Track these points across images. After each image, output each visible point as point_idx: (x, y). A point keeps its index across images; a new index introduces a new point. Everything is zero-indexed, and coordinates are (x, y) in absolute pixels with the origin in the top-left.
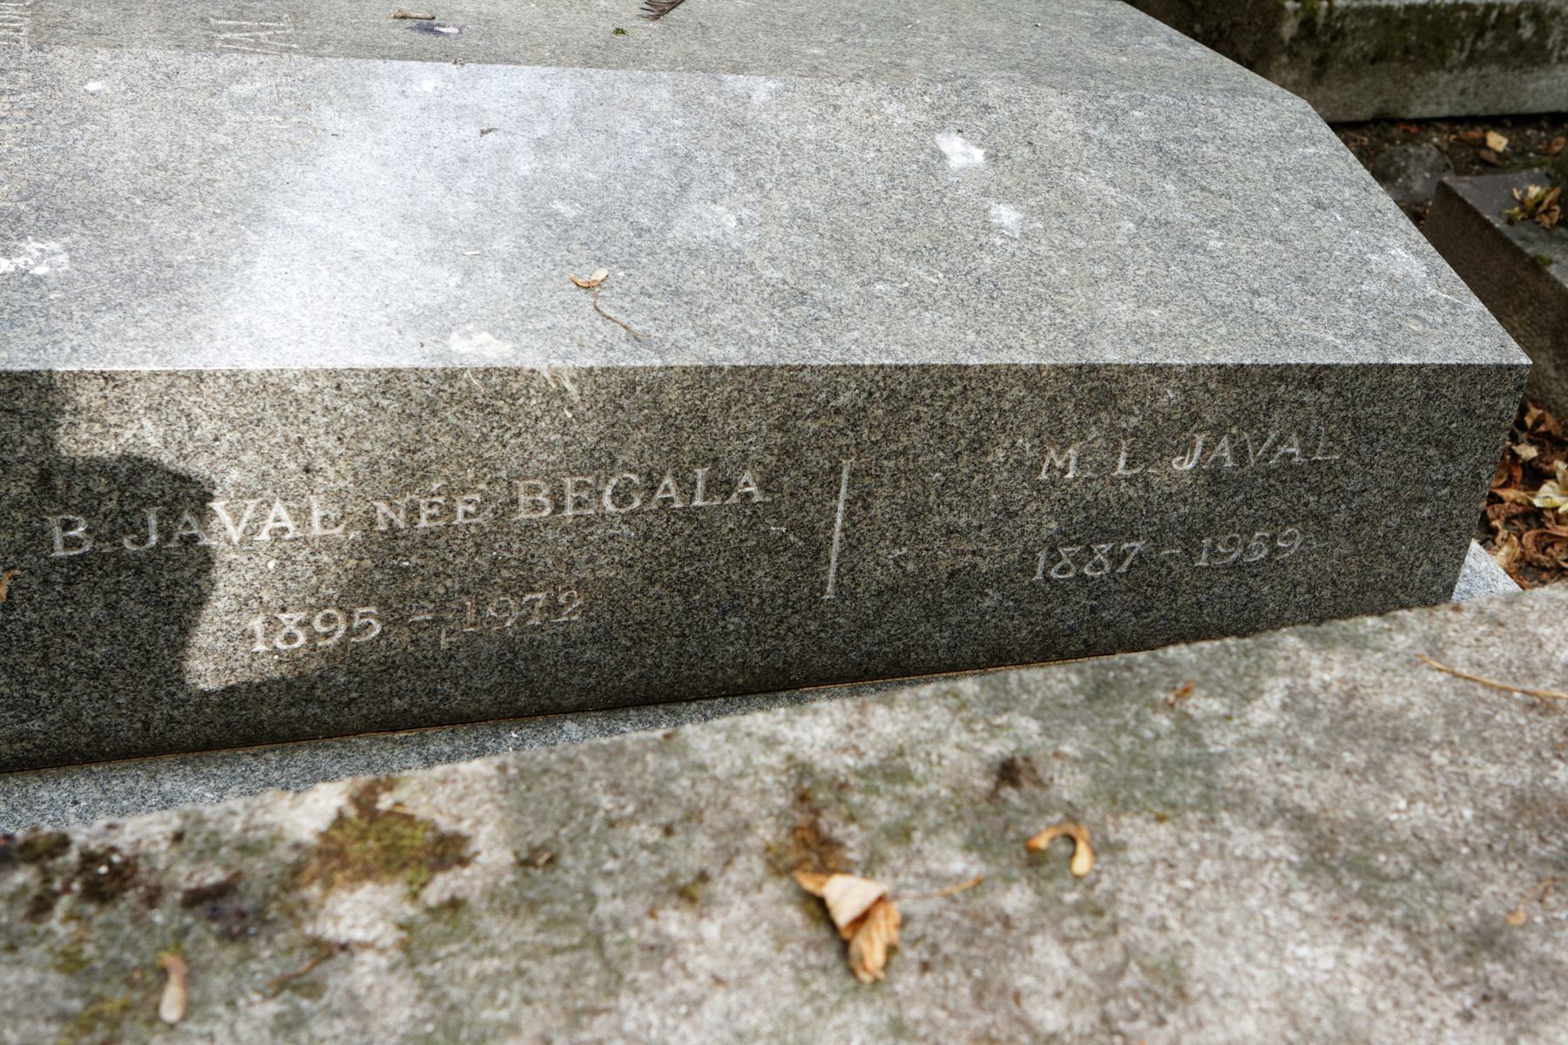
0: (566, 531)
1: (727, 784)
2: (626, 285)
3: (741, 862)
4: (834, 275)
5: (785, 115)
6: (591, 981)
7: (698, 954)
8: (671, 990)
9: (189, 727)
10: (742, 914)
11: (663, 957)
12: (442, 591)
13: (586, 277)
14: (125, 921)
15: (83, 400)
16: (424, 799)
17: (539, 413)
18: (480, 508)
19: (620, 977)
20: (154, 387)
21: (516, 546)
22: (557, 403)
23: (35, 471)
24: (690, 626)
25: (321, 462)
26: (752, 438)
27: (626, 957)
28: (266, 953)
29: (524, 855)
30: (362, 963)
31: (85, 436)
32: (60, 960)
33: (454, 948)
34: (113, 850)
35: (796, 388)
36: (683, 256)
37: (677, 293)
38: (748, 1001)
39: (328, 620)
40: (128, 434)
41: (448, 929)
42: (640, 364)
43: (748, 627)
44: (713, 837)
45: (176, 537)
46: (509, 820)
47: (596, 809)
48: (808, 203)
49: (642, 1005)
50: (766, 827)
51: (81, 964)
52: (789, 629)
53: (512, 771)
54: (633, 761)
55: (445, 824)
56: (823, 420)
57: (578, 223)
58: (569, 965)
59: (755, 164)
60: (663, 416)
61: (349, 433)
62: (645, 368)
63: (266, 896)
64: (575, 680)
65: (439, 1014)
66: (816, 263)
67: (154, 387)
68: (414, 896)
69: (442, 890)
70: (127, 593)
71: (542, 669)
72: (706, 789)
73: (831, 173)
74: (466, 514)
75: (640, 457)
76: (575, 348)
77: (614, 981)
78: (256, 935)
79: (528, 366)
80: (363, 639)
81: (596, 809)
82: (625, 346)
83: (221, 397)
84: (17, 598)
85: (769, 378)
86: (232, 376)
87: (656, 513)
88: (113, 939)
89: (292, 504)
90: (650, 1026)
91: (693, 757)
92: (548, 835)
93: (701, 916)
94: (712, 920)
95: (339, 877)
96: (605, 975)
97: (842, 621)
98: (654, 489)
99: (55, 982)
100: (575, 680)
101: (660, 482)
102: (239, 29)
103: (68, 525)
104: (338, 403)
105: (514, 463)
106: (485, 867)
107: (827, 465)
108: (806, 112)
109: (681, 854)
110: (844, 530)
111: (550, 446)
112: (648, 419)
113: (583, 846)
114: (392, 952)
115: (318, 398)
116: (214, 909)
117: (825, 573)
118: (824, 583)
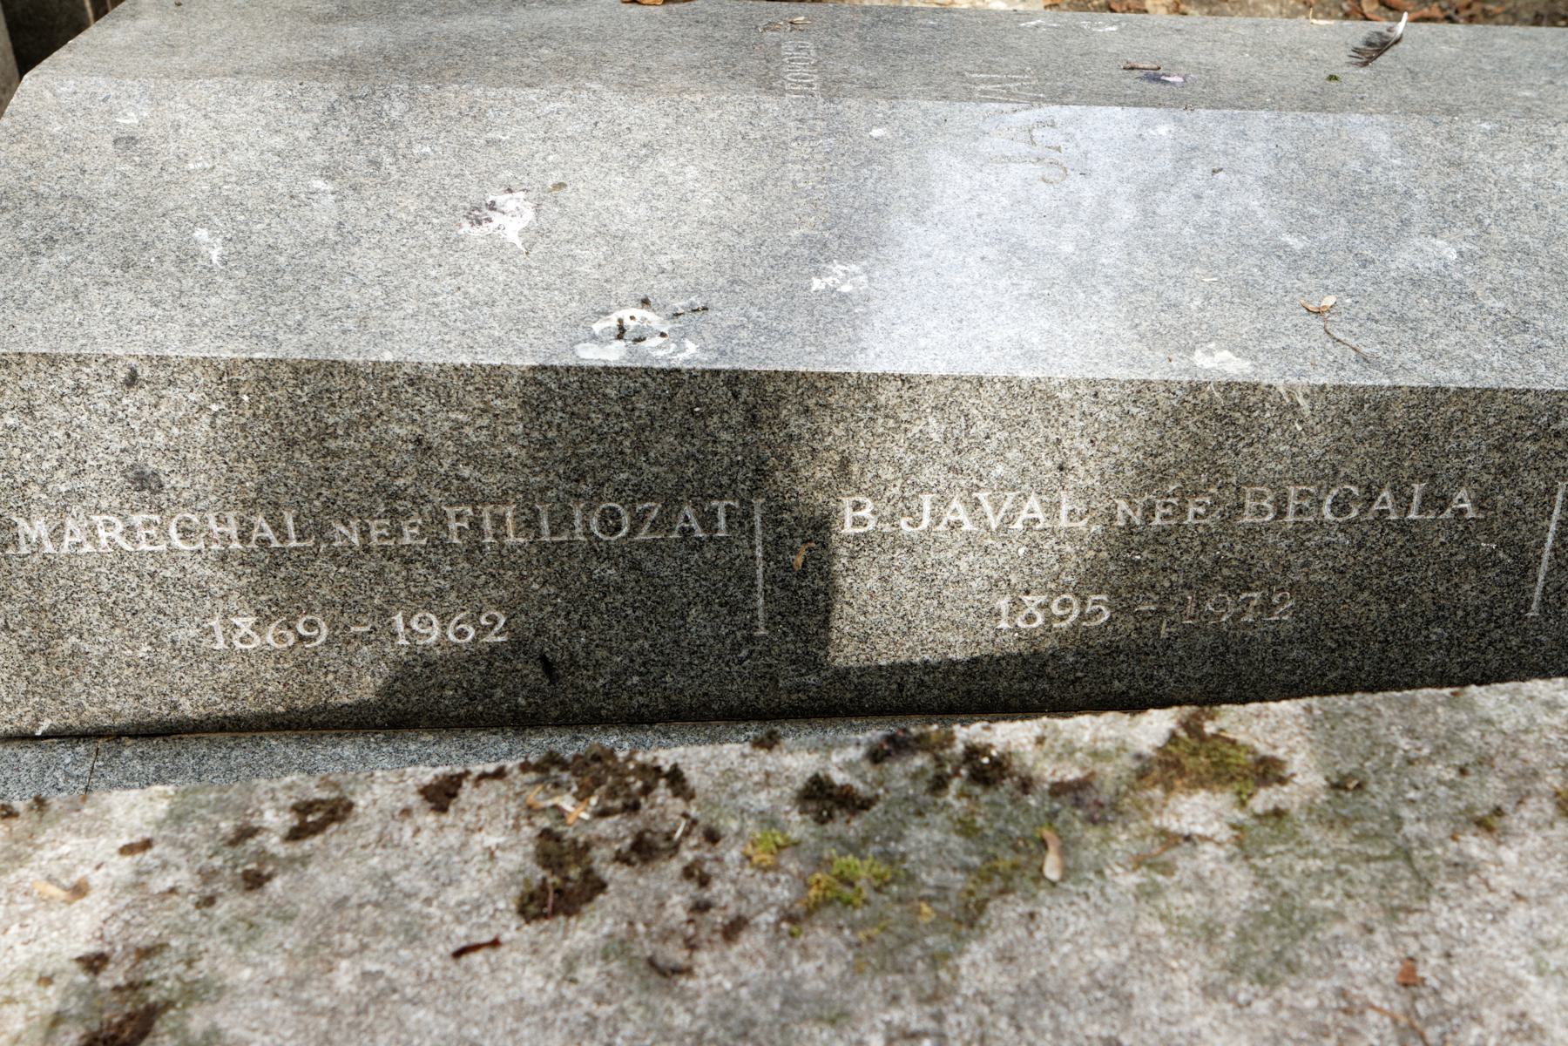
0: (1285, 536)
1: (1515, 736)
2: (1353, 311)
3: (1532, 802)
4: (1555, 306)
5: (1502, 154)
6: (1404, 885)
7: (1499, 873)
8: (1476, 900)
9: (936, 692)
10: (1536, 844)
11: (1467, 874)
12: (1167, 584)
13: (1316, 303)
14: (1006, 802)
15: (882, 399)
16: (1242, 728)
17: (1271, 425)
18: (1209, 511)
19: (1430, 885)
20: (941, 389)
21: (1238, 547)
22: (1289, 416)
23: (837, 458)
24: (1394, 633)
25: (1074, 462)
26: (1471, 457)
27: (1434, 869)
28: (1123, 837)
29: (1335, 780)
30: (1204, 852)
31: (881, 430)
32: (958, 826)
33: (1282, 848)
34: (991, 746)
35: (1517, 411)
36: (1406, 286)
37: (1402, 319)
38: (1548, 915)
39: (1065, 604)
40: (915, 430)
41: (1275, 833)
42: (1370, 383)
43: (1450, 638)
44: (1505, 780)
45: (944, 522)
46: (1320, 751)
47: (1395, 748)
48: (1527, 238)
49: (1451, 909)
50: (1554, 775)
51: (976, 830)
52: (1490, 643)
53: (1317, 712)
54: (1426, 712)
55: (1263, 750)
56: (1543, 442)
57: (1305, 254)
58: (1383, 871)
59: (1472, 201)
60: (1405, 433)
61: (1103, 434)
62: (1374, 387)
63: (1118, 793)
64: (1281, 676)
65: (1273, 898)
66: (1537, 294)
67: (941, 389)
68: (1243, 804)
69: (1266, 802)
70: (898, 569)
71: (1251, 663)
72: (1495, 740)
73: (1550, 209)
74: (1196, 515)
75: (1361, 470)
76: (1308, 367)
77: (1424, 886)
78: (1113, 822)
79: (1266, 382)
80: (1093, 624)
81: (1395, 748)
82: (1355, 367)
83: (996, 400)
84: (810, 568)
85: (1493, 400)
86: (1007, 382)
87: (1372, 523)
88: (998, 815)
89: (1045, 498)
90: (1460, 926)
91: (1480, 713)
92: (1355, 766)
93: (1499, 843)
94: (1510, 848)
95: (1178, 783)
96: (1415, 883)
97: (1544, 638)
98: (1371, 501)
99: (956, 842)
100: (1281, 676)
101: (1378, 494)
102: (991, 81)
103: (857, 506)
104: (1095, 409)
105: (1245, 470)
106: (1301, 787)
107: (1543, 486)
108: (1522, 152)
109: (1476, 792)
110: (1554, 550)
111: (1279, 456)
112: (1373, 435)
113: (1387, 777)
114: (1228, 846)
115: (1077, 404)
116: (1077, 799)
117: (1531, 591)
118: (1529, 601)
